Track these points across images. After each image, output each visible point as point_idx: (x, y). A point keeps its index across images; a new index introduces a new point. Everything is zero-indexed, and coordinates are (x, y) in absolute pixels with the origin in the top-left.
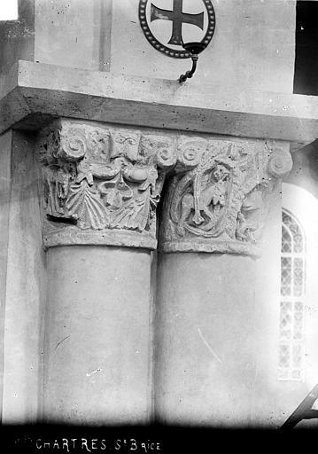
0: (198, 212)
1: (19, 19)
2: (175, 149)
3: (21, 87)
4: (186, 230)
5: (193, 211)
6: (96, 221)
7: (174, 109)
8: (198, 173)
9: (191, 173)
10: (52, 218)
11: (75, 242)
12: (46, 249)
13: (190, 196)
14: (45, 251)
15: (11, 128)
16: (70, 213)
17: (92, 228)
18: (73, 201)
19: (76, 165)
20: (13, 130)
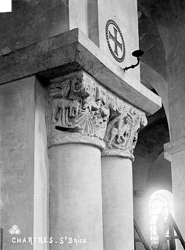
0: (119, 137)
1: (12, 10)
2: (118, 104)
3: (79, 43)
4: (113, 145)
5: (117, 136)
6: (90, 131)
7: (122, 82)
8: (121, 118)
9: (118, 118)
10: (58, 128)
11: (81, 141)
12: (49, 148)
13: (116, 129)
14: (49, 148)
15: (37, 75)
16: (77, 125)
17: (88, 135)
18: (80, 118)
19: (83, 99)
20: (36, 76)
